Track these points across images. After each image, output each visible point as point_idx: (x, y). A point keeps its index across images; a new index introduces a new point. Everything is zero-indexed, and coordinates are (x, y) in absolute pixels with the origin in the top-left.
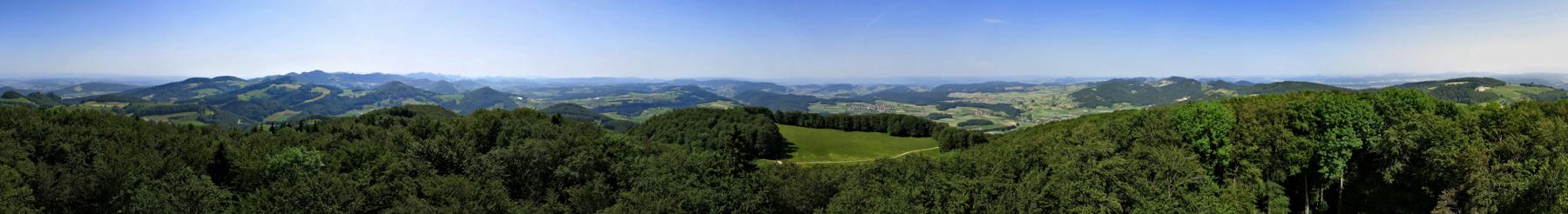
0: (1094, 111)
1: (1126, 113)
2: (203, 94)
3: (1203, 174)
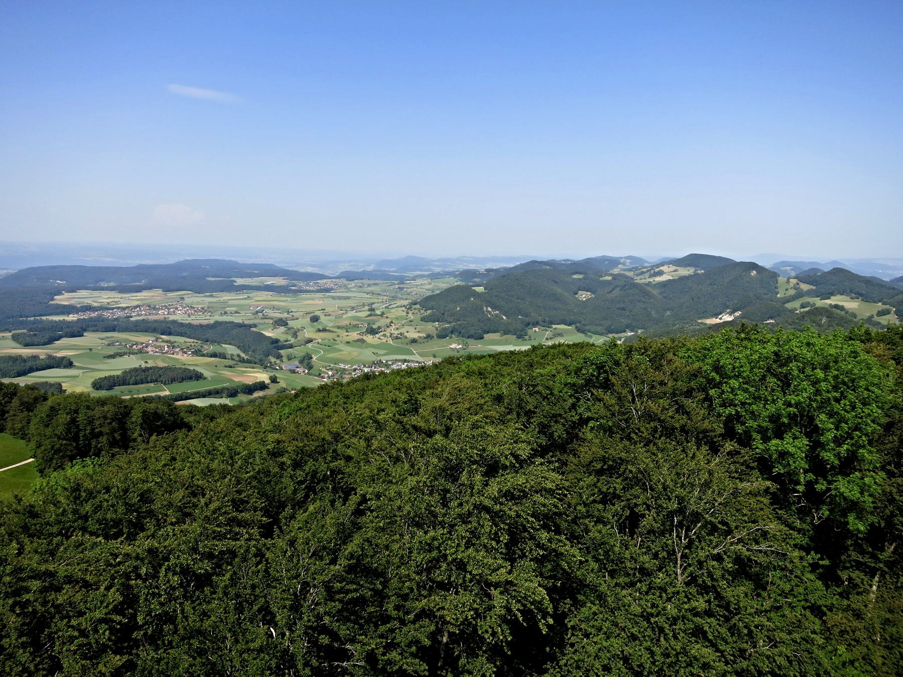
0: (477, 347)
1: (562, 351)
3: (778, 538)
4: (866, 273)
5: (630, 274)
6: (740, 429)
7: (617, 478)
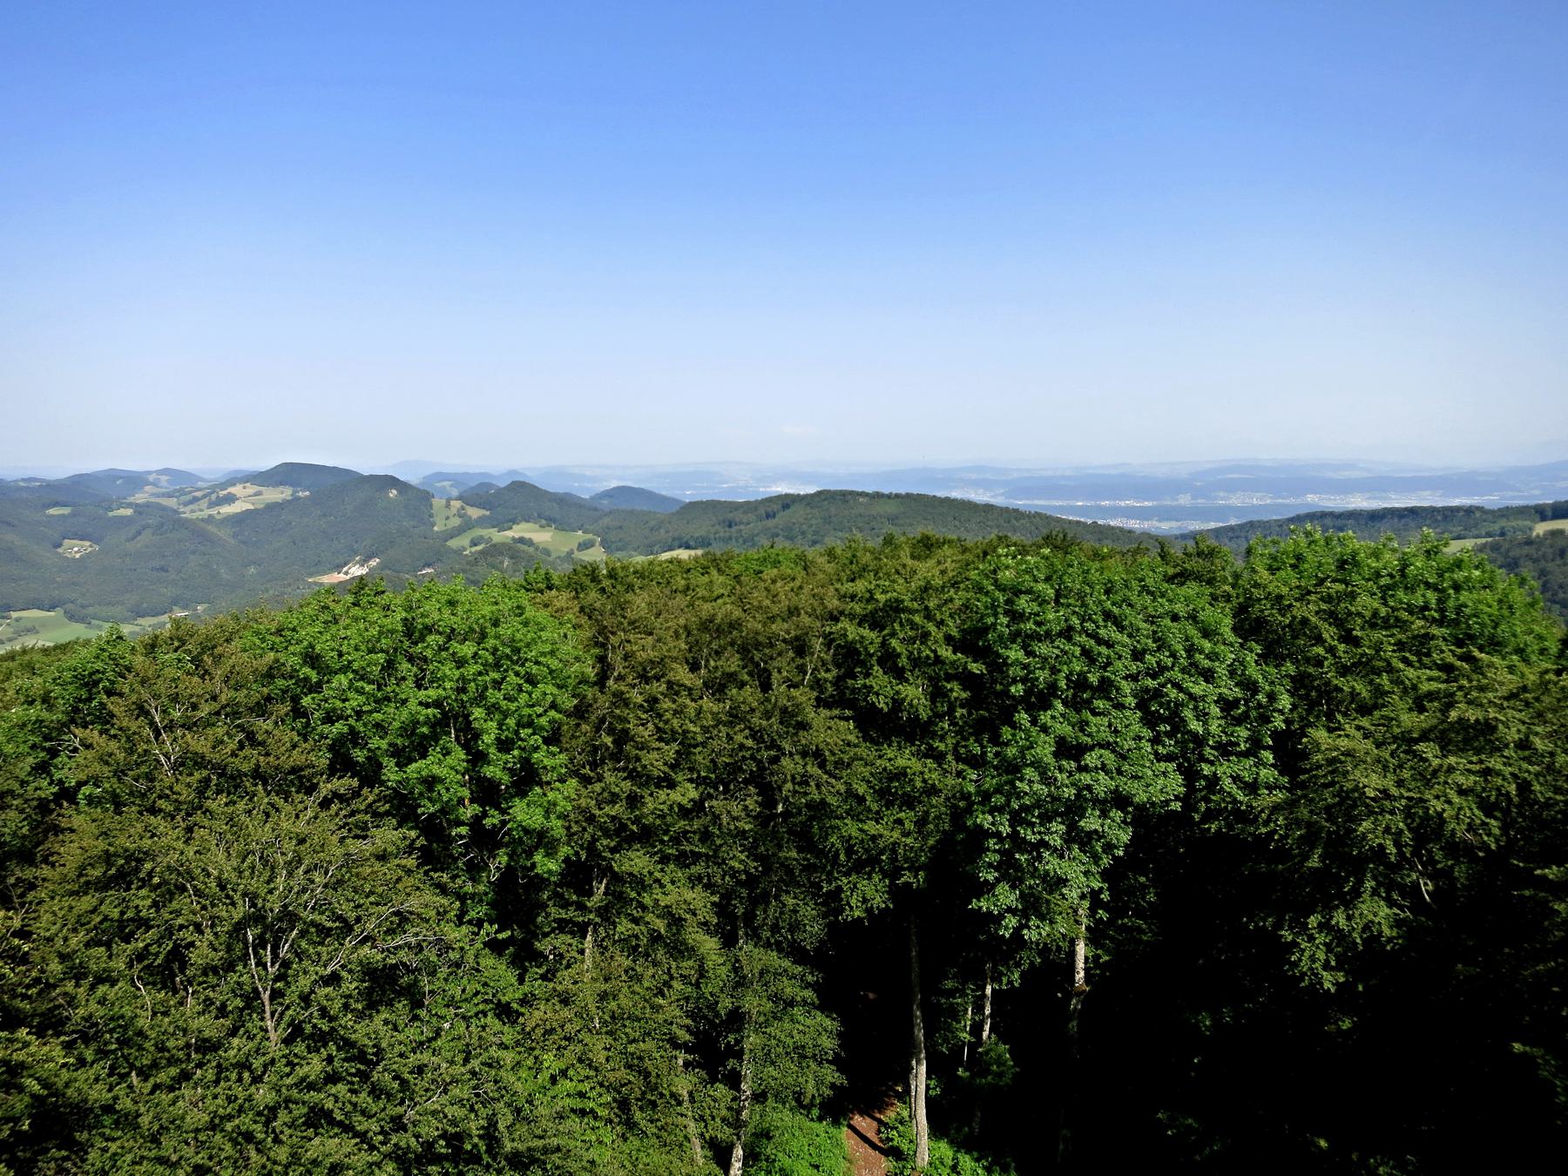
3: (436, 920)
4: (555, 486)
5: (172, 503)
6: (359, 755)
7: (139, 888)
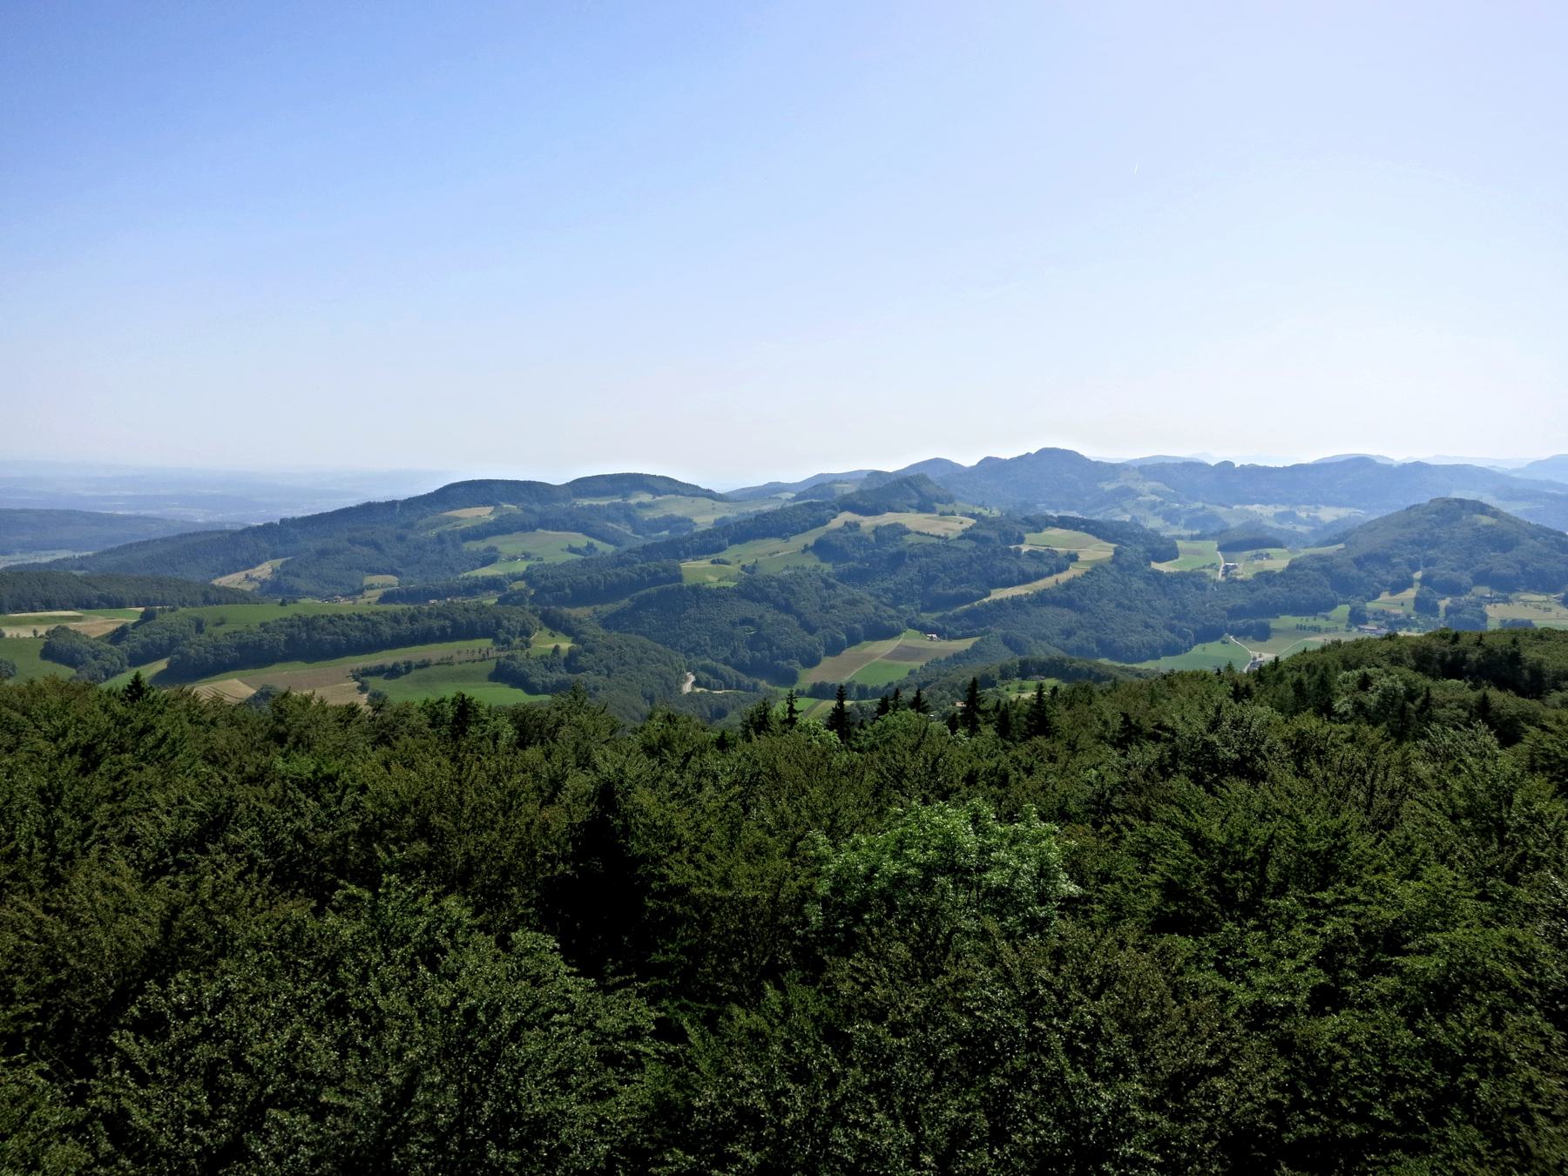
2: (516, 557)
